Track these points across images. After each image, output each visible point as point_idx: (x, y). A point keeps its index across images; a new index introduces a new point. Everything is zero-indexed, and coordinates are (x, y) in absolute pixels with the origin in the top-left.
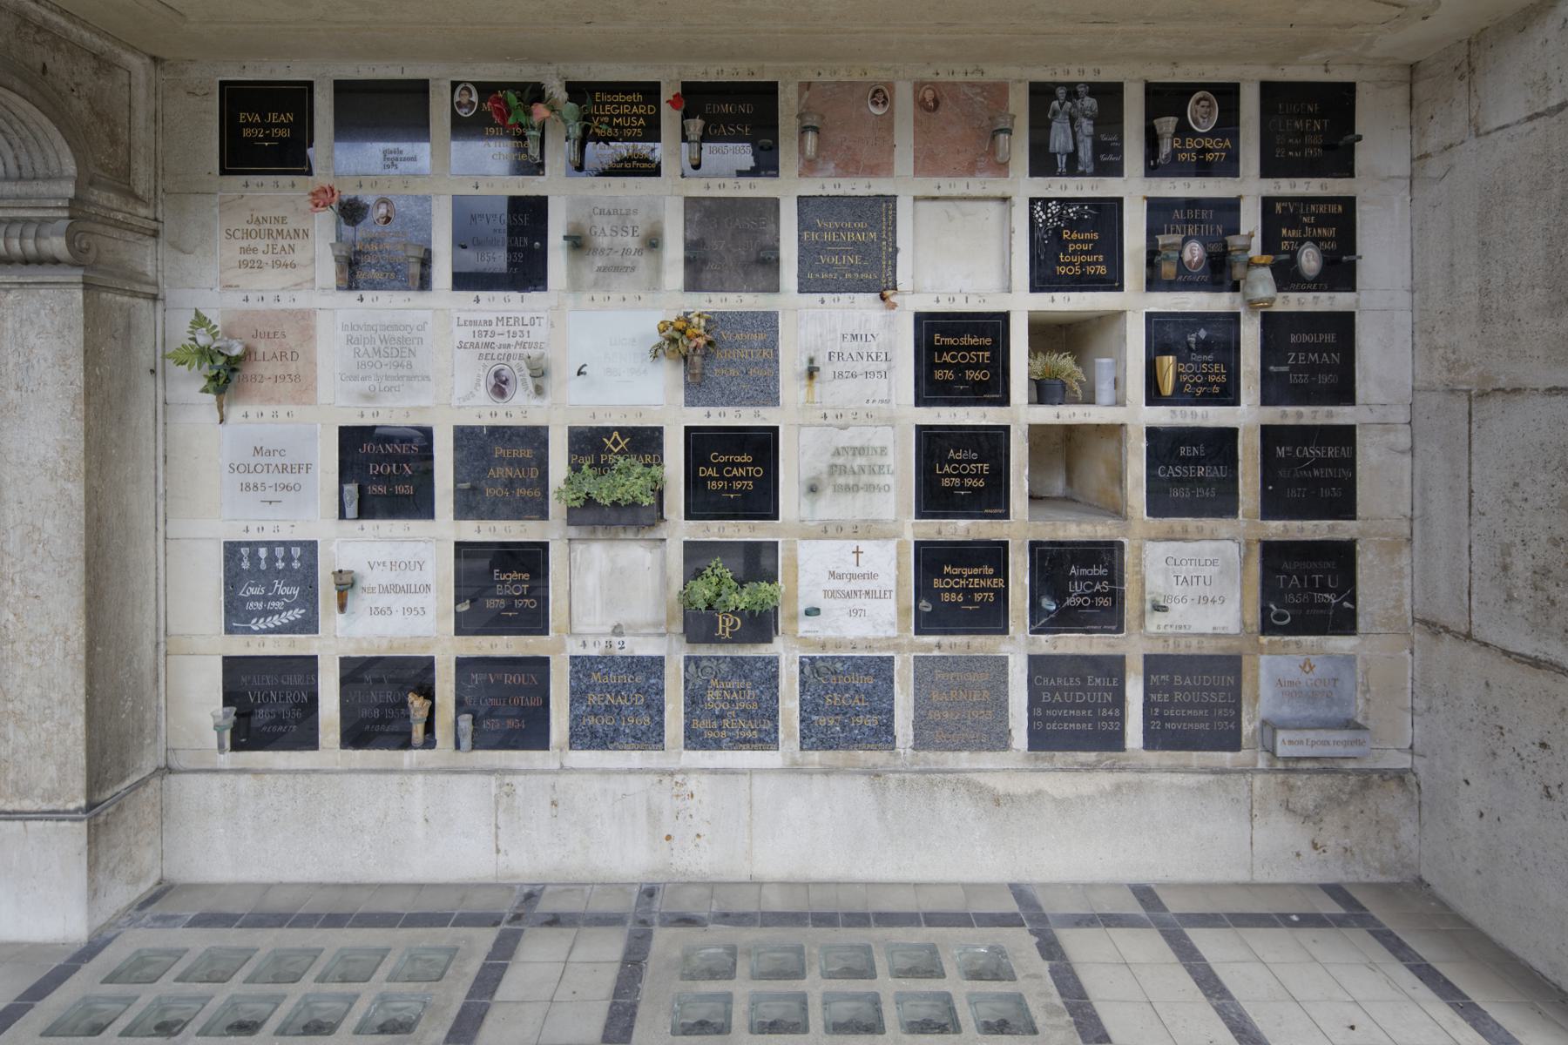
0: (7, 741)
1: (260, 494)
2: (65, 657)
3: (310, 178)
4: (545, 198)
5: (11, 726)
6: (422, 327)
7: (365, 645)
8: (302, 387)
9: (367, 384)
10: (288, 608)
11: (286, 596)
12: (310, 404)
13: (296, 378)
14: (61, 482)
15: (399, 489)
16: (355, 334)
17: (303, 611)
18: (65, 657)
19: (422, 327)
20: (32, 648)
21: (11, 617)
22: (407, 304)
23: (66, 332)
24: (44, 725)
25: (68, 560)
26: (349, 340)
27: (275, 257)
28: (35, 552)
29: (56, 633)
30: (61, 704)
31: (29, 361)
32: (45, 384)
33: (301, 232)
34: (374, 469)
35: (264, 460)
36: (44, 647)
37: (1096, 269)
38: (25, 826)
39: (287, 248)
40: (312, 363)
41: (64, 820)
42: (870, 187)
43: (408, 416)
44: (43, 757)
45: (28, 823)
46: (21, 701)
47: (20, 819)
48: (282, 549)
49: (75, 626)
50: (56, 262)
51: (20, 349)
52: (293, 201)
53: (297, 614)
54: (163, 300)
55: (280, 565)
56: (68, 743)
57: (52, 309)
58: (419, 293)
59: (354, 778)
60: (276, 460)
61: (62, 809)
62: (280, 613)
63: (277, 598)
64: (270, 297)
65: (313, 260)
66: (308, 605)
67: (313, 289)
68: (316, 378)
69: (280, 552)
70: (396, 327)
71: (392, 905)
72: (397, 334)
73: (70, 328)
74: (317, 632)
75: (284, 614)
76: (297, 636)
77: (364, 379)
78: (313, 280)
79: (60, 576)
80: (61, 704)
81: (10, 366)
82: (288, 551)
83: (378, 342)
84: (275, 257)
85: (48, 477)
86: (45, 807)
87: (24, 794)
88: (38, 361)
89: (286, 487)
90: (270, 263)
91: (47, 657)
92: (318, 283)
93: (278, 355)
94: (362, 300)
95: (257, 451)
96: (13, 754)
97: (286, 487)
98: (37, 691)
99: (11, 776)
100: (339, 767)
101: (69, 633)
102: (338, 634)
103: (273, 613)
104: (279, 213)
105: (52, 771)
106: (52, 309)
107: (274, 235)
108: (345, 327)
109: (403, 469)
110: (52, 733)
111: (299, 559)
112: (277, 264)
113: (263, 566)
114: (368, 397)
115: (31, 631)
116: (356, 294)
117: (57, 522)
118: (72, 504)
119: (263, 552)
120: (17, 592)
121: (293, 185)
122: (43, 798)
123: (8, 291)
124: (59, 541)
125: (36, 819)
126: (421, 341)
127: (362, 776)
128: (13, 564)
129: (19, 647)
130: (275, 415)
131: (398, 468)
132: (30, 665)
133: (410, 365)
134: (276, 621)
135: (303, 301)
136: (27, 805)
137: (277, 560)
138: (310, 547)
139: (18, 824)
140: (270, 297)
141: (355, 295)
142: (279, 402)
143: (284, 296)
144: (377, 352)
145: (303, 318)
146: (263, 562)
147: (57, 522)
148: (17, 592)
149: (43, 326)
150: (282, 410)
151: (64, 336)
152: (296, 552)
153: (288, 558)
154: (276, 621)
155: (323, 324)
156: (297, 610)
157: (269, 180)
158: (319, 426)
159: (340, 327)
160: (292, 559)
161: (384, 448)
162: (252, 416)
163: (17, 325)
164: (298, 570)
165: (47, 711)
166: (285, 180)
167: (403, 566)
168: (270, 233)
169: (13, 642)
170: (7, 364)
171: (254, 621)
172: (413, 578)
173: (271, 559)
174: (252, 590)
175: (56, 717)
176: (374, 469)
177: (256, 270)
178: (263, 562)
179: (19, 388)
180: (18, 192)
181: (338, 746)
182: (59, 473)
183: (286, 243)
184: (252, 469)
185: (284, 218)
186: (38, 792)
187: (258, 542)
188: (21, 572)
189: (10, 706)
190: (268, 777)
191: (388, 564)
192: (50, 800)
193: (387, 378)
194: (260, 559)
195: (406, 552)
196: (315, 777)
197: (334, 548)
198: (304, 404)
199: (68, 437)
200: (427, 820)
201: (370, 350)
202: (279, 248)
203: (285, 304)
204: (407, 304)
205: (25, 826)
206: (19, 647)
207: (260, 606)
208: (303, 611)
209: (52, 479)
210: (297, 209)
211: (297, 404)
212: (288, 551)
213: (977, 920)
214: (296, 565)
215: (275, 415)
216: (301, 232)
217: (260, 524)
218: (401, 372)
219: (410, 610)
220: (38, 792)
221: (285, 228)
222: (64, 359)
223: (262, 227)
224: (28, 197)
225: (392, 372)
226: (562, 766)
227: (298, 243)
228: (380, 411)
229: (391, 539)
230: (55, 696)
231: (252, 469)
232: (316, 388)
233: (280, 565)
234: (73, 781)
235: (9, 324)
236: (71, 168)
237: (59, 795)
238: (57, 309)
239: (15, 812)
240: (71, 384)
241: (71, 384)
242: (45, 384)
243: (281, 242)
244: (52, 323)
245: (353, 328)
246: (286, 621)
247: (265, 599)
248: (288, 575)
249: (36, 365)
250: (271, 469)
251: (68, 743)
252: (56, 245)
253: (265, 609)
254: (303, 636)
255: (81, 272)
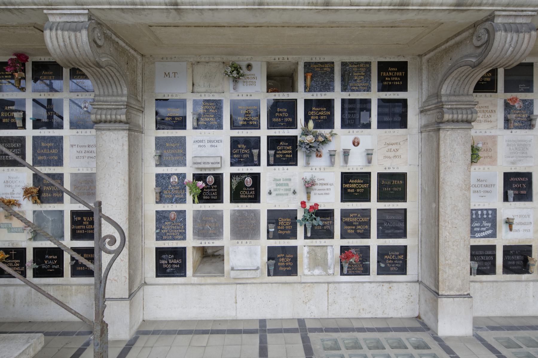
0: (446, 273)
1: (479, 194)
2: (464, 246)
3: (496, 94)
4: (296, 100)
5: (447, 269)
6: (530, 141)
7: (511, 241)
8: (493, 160)
9: (513, 159)
10: (487, 230)
11: (487, 226)
12: (495, 165)
13: (491, 157)
14: (464, 191)
15: (522, 192)
16: (509, 143)
17: (492, 231)
18: (464, 246)
19: (530, 141)
20: (454, 244)
21: (448, 234)
22: (526, 134)
23: (466, 144)
24: (457, 268)
25: (466, 216)
26: (508, 145)
27: (485, 119)
28: (455, 213)
29: (461, 239)
30: (463, 261)
31: (454, 153)
32: (459, 160)
33: (493, 111)
34: (514, 186)
35: (481, 183)
36: (458, 243)
37: (288, 119)
38: (454, 299)
39: (489, 116)
40: (496, 152)
41: (466, 297)
42: (78, 96)
43: (525, 169)
44: (457, 278)
45: (455, 299)
46: (451, 260)
47: (452, 297)
48: (491, 211)
49: (467, 236)
50: (121, 122)
51: (451, 149)
52: (491, 101)
53: (490, 232)
54: (144, 133)
55: (485, 216)
56: (465, 273)
57: (461, 137)
58: (529, 130)
59: (511, 283)
60: (484, 183)
61: (463, 294)
62: (485, 231)
63: (484, 227)
64: (483, 131)
65: (497, 120)
66: (494, 229)
67: (497, 129)
68: (497, 157)
69: (485, 212)
70: (522, 141)
71: (241, 327)
72: (523, 143)
73: (467, 142)
74: (496, 237)
75: (486, 232)
76: (490, 239)
77: (512, 157)
78: (497, 126)
79: (463, 221)
80: (463, 261)
81: (448, 154)
82: (487, 212)
83: (517, 146)
84: (485, 119)
85: (460, 189)
86: (458, 294)
87: (451, 289)
88: (457, 153)
89: (487, 192)
90: (484, 121)
91: (459, 246)
92: (498, 127)
93: (485, 150)
94: (512, 132)
95: (478, 180)
96: (448, 277)
97: (487, 192)
98: (456, 257)
99: (447, 284)
100: (502, 280)
101: (466, 239)
102: (503, 238)
103: (482, 231)
104: (486, 105)
105: (460, 282)
106: (461, 137)
107: (485, 112)
108: (506, 141)
109: (523, 186)
110: (460, 270)
111: (491, 214)
112: (486, 121)
113: (480, 217)
114: (513, 163)
115: (454, 238)
116: (510, 131)
117: (462, 204)
118: (467, 198)
119: (480, 212)
120: (450, 226)
121: (491, 96)
122: (457, 291)
123: (448, 131)
124: (463, 210)
125: (457, 297)
126: (530, 145)
127: (514, 283)
128: (449, 217)
129: (450, 243)
130: (484, 169)
131: (521, 185)
132: (453, 249)
133: (526, 153)
134: (483, 234)
135: (494, 132)
136: (452, 293)
137: (484, 215)
138: (494, 211)
139: (451, 299)
140: (483, 131)
141: (509, 131)
142: (485, 165)
143: (488, 131)
144: (516, 149)
145: (493, 138)
146: (480, 215)
147: (462, 204)
148: (450, 226)
149: (459, 142)
150: (486, 167)
151: (465, 145)
152: (490, 212)
153: (488, 214)
154: (483, 234)
155: (499, 139)
156: (490, 231)
157: (483, 94)
158: (498, 172)
159: (505, 141)
160: (489, 214)
161: (517, 179)
162: (486, 169)
163: (451, 142)
164: (491, 218)
165: (458, 264)
166: (488, 94)
167: (523, 216)
168: (483, 111)
169: (448, 242)
170: (447, 154)
171: (477, 234)
172: (526, 220)
173: (482, 214)
174: (476, 224)
175: (461, 265)
176: (514, 186)
177: (479, 123)
178: (480, 215)
179: (451, 161)
180: (456, 99)
181: (502, 273)
182: (463, 188)
183: (488, 114)
184: (476, 186)
185: (488, 106)
186: (455, 289)
187: (478, 209)
188: (451, 220)
189: (447, 262)
190: (485, 283)
191: (519, 216)
192: (459, 291)
193: (519, 157)
194: (479, 214)
195: (525, 212)
196: (499, 283)
197: (502, 211)
198: (493, 165)
199: (466, 177)
200: (534, 296)
201: (514, 148)
202: (486, 116)
203: (488, 134)
204: (526, 134)
205: (454, 299)
206: (450, 243)
207: (478, 229)
208: (492, 231)
209: (461, 190)
210: (492, 104)
211: (491, 165)
212: (487, 212)
213: (325, 330)
214: (490, 216)
215: (484, 169)
216: (493, 111)
217: (479, 203)
218: (524, 155)
219: (525, 230)
220: (455, 289)
221: (488, 109)
222: (465, 152)
223: (481, 109)
224: (107, 102)
225: (521, 155)
226: (145, 282)
227: (492, 114)
228: (517, 168)
229: (520, 208)
230: (461, 259)
231: (476, 186)
232: (497, 160)
233: (485, 216)
234: (466, 285)
235: (448, 141)
236: (125, 92)
237: (462, 290)
238: (463, 136)
239: (448, 295)
240: (467, 160)
241: (467, 160)
242: (459, 160)
243: (487, 114)
244: (461, 141)
245: (509, 141)
246: (487, 234)
247: (480, 227)
248: (488, 220)
249: (456, 154)
250: (483, 186)
251: (465, 273)
252: (123, 118)
253: (480, 230)
254: (492, 239)
255: (127, 125)
